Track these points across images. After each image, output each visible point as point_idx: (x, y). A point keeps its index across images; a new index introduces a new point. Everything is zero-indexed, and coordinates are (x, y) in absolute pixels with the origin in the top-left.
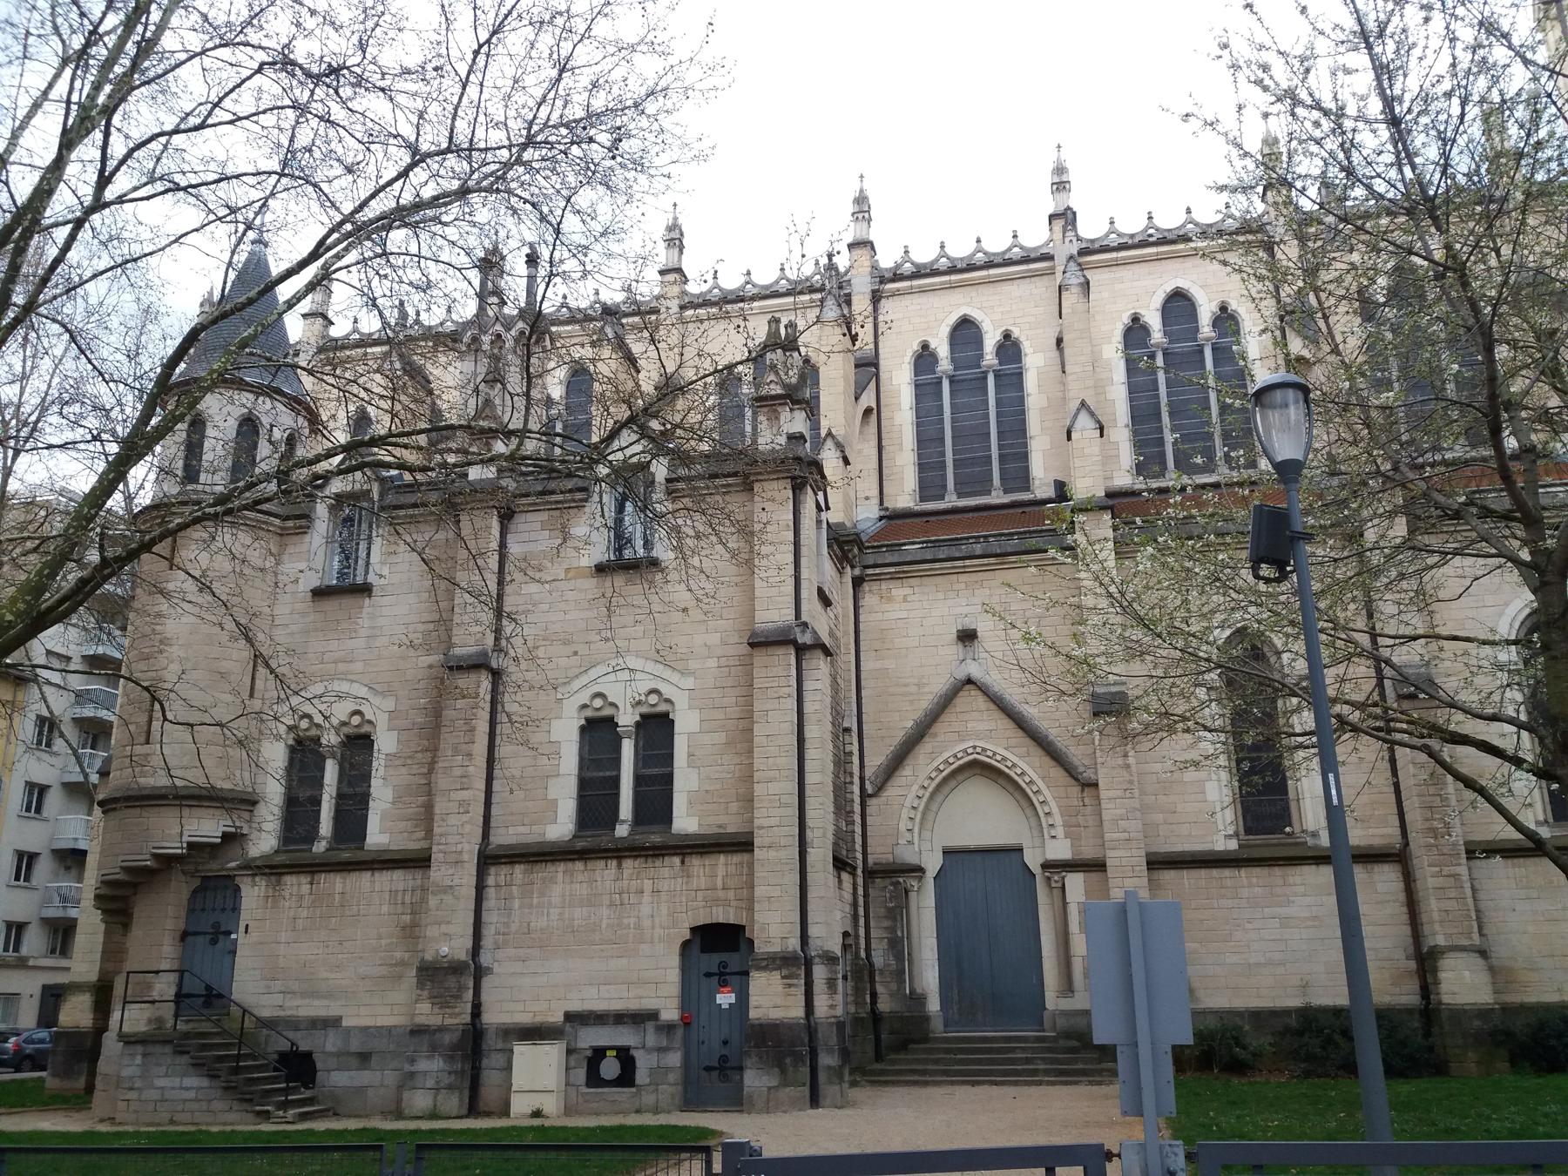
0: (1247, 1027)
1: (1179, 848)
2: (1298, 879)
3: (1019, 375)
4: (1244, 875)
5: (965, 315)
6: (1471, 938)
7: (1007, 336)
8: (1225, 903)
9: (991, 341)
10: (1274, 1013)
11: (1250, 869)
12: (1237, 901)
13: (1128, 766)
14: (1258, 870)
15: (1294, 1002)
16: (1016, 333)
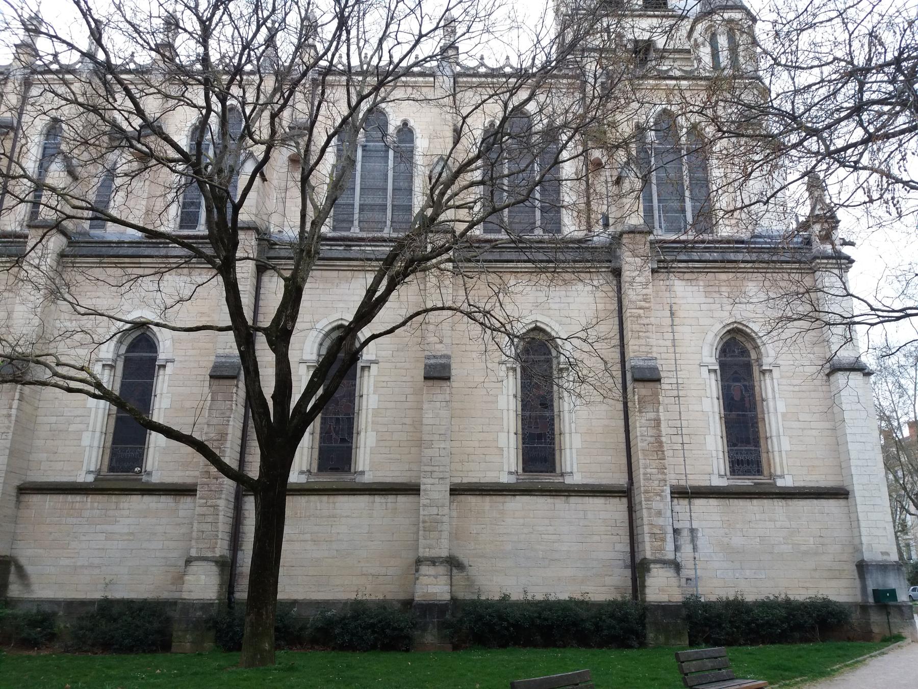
0: (61, 613)
1: (52, 479)
2: (126, 505)
3: (412, 151)
4: (90, 501)
6: (214, 552)
7: (405, 123)
8: (71, 520)
10: (83, 603)
11: (95, 496)
12: (80, 519)
13: (9, 416)
14: (100, 497)
15: (98, 595)
16: (412, 123)
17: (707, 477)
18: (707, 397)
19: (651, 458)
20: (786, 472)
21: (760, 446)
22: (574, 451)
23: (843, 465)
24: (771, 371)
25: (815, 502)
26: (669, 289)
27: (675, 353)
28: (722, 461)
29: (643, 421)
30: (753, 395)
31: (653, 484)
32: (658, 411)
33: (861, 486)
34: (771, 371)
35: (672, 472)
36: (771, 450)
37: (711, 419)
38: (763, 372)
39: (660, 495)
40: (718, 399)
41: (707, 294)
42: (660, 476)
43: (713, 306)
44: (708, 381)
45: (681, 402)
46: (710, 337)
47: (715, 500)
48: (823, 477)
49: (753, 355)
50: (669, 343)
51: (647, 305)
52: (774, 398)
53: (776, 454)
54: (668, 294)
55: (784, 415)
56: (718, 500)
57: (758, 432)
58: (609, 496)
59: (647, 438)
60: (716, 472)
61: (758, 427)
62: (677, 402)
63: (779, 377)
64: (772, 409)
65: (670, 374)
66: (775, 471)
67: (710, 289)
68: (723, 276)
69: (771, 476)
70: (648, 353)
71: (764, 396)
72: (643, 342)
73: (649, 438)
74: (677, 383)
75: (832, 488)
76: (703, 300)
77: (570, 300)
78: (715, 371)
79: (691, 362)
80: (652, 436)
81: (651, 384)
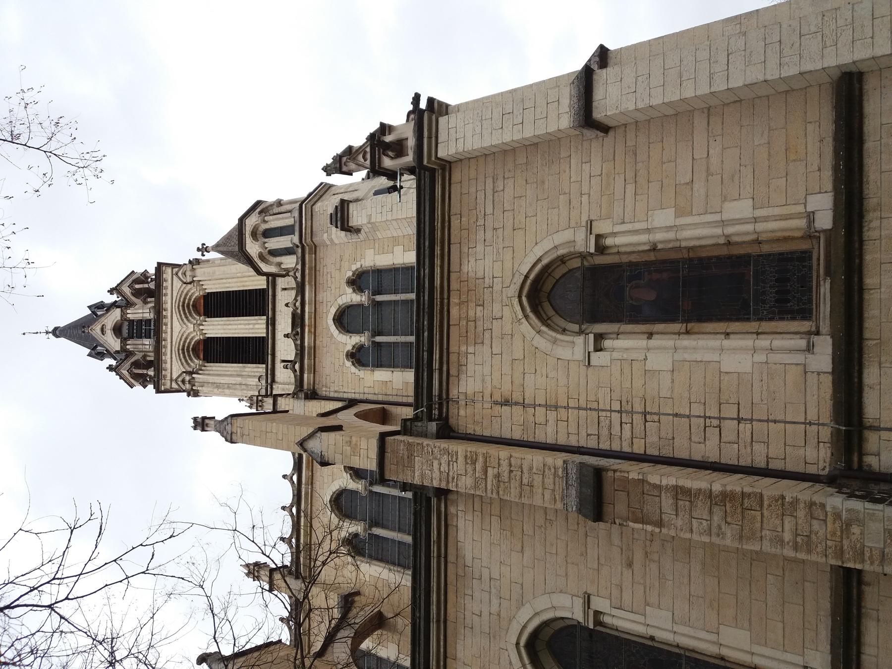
5: (334, 320)
9: (351, 297)
17: (812, 379)
18: (646, 359)
19: (758, 525)
20: (800, 209)
21: (749, 256)
22: (757, 649)
23: (783, 87)
24: (599, 237)
25: (870, 145)
26: (471, 401)
27: (567, 408)
28: (778, 342)
29: (679, 523)
30: (647, 264)
31: (821, 533)
32: (659, 487)
33: (826, 51)
34: (599, 237)
35: (802, 451)
36: (754, 237)
37: (687, 357)
38: (601, 249)
39: (849, 525)
40: (650, 335)
41: (478, 341)
42: (801, 513)
43: (496, 331)
44: (616, 355)
45: (655, 410)
46: (541, 343)
47: (866, 372)
48: (810, 127)
49: (576, 263)
50: (552, 415)
51: (481, 459)
52: (648, 231)
53: (761, 227)
54: (478, 405)
55: (680, 212)
56: (866, 363)
57: (718, 258)
58: (859, 607)
59: (715, 524)
60: (799, 358)
61: (710, 258)
62: (656, 418)
63: (609, 221)
64: (671, 235)
65: (605, 423)
66: (798, 229)
67: (471, 335)
68: (454, 311)
69: (811, 235)
70: (555, 475)
71: (646, 248)
72: (538, 479)
73: (716, 518)
74: (620, 412)
75: (837, 108)
76: (486, 349)
77: (486, 574)
78: (599, 337)
79: (583, 382)
80: (711, 512)
81: (608, 489)
